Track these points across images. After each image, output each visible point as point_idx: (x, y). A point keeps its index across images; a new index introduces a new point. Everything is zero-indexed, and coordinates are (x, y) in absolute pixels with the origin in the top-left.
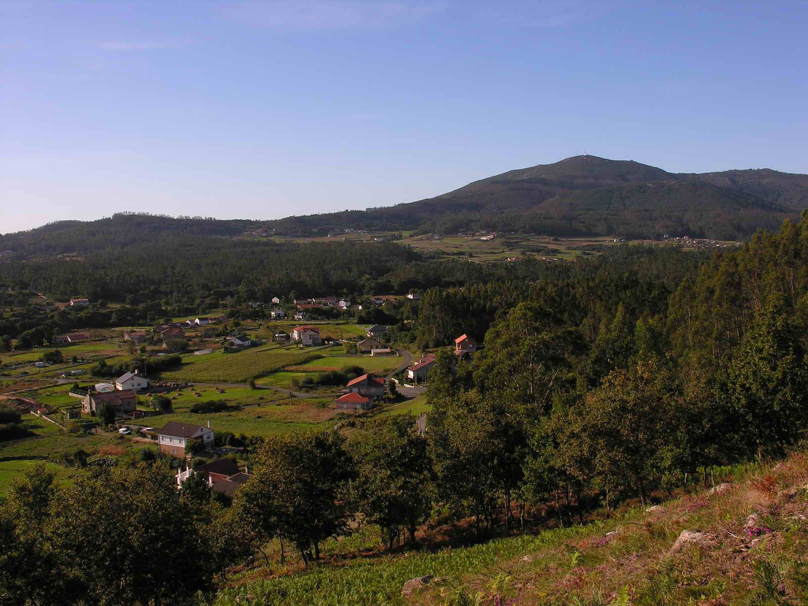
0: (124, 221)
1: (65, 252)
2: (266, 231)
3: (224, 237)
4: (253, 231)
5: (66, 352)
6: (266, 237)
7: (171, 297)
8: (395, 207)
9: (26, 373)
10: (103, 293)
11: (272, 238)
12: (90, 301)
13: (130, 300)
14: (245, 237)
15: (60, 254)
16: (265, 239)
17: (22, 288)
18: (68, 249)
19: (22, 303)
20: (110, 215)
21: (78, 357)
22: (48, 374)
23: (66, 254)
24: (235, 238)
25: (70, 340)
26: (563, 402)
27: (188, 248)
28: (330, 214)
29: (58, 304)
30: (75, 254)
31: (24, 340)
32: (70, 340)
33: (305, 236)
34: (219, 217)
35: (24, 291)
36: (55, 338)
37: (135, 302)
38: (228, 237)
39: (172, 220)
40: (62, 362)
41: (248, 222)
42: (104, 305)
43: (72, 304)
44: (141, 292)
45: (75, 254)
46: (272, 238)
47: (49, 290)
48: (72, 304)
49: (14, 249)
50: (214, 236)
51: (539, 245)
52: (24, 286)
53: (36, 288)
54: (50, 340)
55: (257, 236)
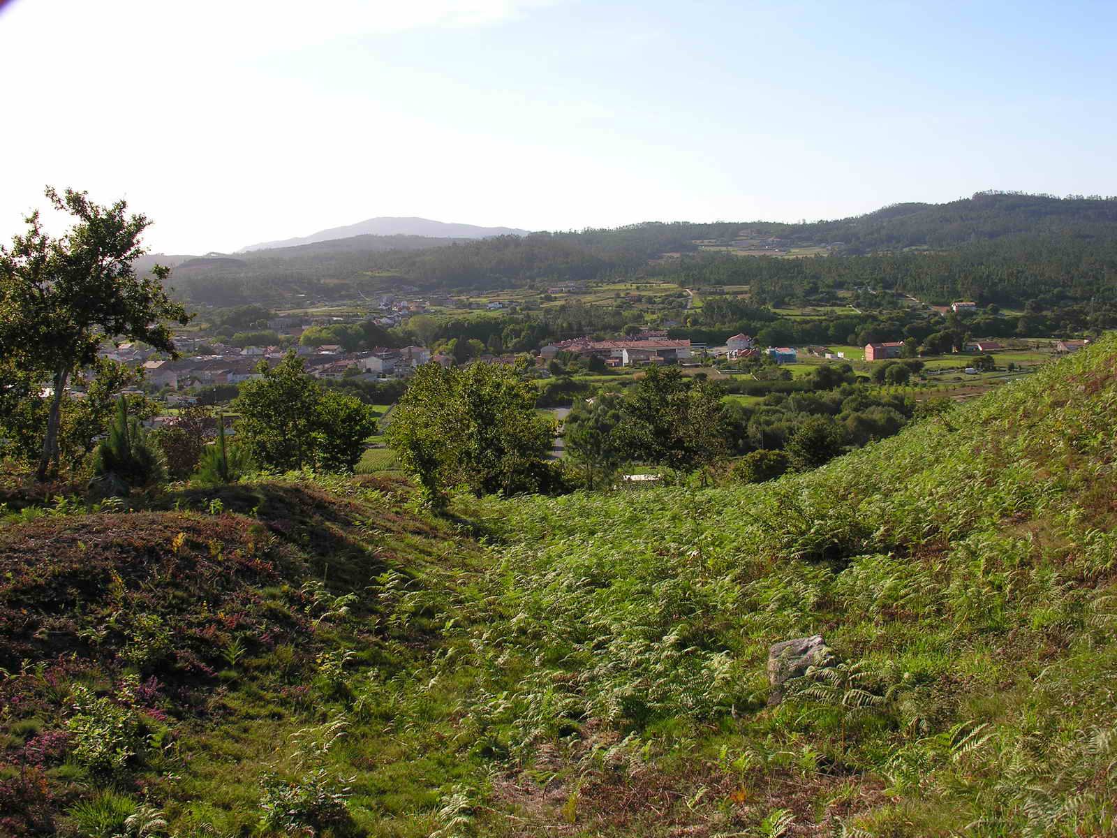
0: (988, 204)
1: (911, 245)
5: (998, 358)
7: (1087, 304)
8: (560, 235)
10: (992, 297)
18: (917, 240)
19: (894, 305)
20: (969, 195)
22: (993, 380)
25: (981, 349)
28: (540, 241)
29: (934, 309)
30: (925, 247)
31: (932, 344)
32: (981, 349)
34: (830, 218)
39: (1059, 200)
40: (994, 369)
42: (995, 311)
43: (954, 308)
44: (1042, 296)
45: (925, 247)
47: (919, 290)
48: (954, 308)
51: (598, 377)
52: (887, 285)
53: (904, 287)
54: (959, 348)
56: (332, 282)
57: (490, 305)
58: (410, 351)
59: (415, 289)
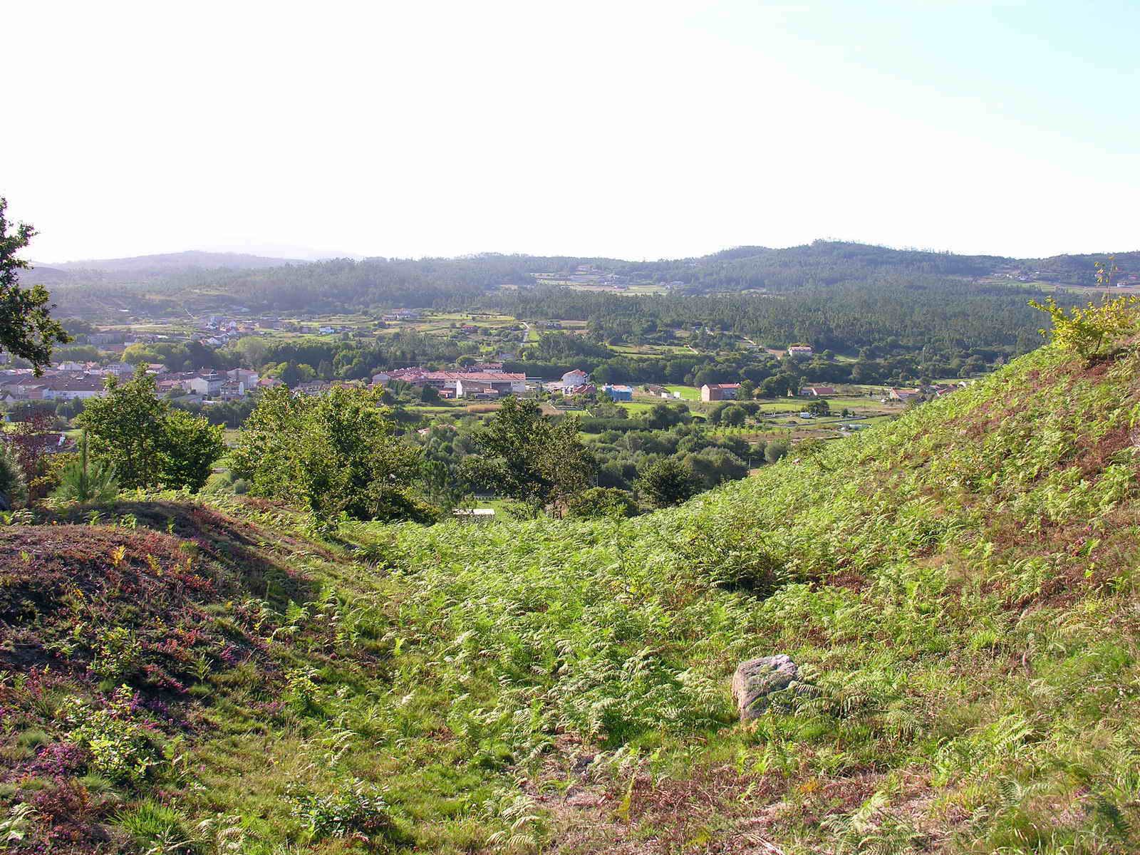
2: (1026, 274)
3: (965, 279)
4: (1007, 273)
5: (833, 404)
6: (1026, 282)
9: (795, 422)
10: (828, 342)
11: (1036, 284)
12: (813, 351)
13: (865, 353)
14: (994, 280)
15: (744, 290)
16: (1026, 286)
17: (723, 329)
18: (756, 283)
19: (731, 347)
21: (849, 412)
22: (828, 425)
23: (752, 290)
24: (981, 282)
25: (815, 394)
26: (73, 810)
27: (920, 291)
29: (771, 352)
30: (764, 290)
31: (768, 387)
33: (1082, 285)
35: (726, 332)
36: (801, 389)
37: (872, 355)
38: (971, 279)
39: (895, 251)
40: (828, 415)
41: (1001, 260)
42: (830, 357)
44: (876, 344)
45: (764, 290)
46: (1036, 284)
47: (757, 333)
49: (686, 280)
50: (951, 277)
54: (794, 392)
55: (1011, 279)
56: (157, 298)
57: (321, 330)
58: (237, 374)
59: (244, 310)
